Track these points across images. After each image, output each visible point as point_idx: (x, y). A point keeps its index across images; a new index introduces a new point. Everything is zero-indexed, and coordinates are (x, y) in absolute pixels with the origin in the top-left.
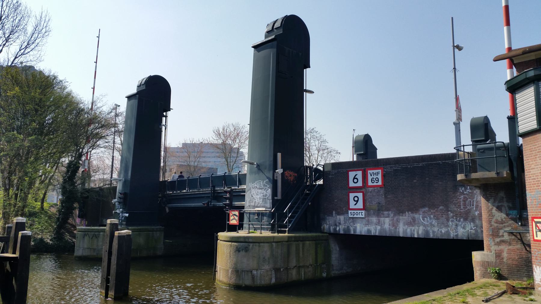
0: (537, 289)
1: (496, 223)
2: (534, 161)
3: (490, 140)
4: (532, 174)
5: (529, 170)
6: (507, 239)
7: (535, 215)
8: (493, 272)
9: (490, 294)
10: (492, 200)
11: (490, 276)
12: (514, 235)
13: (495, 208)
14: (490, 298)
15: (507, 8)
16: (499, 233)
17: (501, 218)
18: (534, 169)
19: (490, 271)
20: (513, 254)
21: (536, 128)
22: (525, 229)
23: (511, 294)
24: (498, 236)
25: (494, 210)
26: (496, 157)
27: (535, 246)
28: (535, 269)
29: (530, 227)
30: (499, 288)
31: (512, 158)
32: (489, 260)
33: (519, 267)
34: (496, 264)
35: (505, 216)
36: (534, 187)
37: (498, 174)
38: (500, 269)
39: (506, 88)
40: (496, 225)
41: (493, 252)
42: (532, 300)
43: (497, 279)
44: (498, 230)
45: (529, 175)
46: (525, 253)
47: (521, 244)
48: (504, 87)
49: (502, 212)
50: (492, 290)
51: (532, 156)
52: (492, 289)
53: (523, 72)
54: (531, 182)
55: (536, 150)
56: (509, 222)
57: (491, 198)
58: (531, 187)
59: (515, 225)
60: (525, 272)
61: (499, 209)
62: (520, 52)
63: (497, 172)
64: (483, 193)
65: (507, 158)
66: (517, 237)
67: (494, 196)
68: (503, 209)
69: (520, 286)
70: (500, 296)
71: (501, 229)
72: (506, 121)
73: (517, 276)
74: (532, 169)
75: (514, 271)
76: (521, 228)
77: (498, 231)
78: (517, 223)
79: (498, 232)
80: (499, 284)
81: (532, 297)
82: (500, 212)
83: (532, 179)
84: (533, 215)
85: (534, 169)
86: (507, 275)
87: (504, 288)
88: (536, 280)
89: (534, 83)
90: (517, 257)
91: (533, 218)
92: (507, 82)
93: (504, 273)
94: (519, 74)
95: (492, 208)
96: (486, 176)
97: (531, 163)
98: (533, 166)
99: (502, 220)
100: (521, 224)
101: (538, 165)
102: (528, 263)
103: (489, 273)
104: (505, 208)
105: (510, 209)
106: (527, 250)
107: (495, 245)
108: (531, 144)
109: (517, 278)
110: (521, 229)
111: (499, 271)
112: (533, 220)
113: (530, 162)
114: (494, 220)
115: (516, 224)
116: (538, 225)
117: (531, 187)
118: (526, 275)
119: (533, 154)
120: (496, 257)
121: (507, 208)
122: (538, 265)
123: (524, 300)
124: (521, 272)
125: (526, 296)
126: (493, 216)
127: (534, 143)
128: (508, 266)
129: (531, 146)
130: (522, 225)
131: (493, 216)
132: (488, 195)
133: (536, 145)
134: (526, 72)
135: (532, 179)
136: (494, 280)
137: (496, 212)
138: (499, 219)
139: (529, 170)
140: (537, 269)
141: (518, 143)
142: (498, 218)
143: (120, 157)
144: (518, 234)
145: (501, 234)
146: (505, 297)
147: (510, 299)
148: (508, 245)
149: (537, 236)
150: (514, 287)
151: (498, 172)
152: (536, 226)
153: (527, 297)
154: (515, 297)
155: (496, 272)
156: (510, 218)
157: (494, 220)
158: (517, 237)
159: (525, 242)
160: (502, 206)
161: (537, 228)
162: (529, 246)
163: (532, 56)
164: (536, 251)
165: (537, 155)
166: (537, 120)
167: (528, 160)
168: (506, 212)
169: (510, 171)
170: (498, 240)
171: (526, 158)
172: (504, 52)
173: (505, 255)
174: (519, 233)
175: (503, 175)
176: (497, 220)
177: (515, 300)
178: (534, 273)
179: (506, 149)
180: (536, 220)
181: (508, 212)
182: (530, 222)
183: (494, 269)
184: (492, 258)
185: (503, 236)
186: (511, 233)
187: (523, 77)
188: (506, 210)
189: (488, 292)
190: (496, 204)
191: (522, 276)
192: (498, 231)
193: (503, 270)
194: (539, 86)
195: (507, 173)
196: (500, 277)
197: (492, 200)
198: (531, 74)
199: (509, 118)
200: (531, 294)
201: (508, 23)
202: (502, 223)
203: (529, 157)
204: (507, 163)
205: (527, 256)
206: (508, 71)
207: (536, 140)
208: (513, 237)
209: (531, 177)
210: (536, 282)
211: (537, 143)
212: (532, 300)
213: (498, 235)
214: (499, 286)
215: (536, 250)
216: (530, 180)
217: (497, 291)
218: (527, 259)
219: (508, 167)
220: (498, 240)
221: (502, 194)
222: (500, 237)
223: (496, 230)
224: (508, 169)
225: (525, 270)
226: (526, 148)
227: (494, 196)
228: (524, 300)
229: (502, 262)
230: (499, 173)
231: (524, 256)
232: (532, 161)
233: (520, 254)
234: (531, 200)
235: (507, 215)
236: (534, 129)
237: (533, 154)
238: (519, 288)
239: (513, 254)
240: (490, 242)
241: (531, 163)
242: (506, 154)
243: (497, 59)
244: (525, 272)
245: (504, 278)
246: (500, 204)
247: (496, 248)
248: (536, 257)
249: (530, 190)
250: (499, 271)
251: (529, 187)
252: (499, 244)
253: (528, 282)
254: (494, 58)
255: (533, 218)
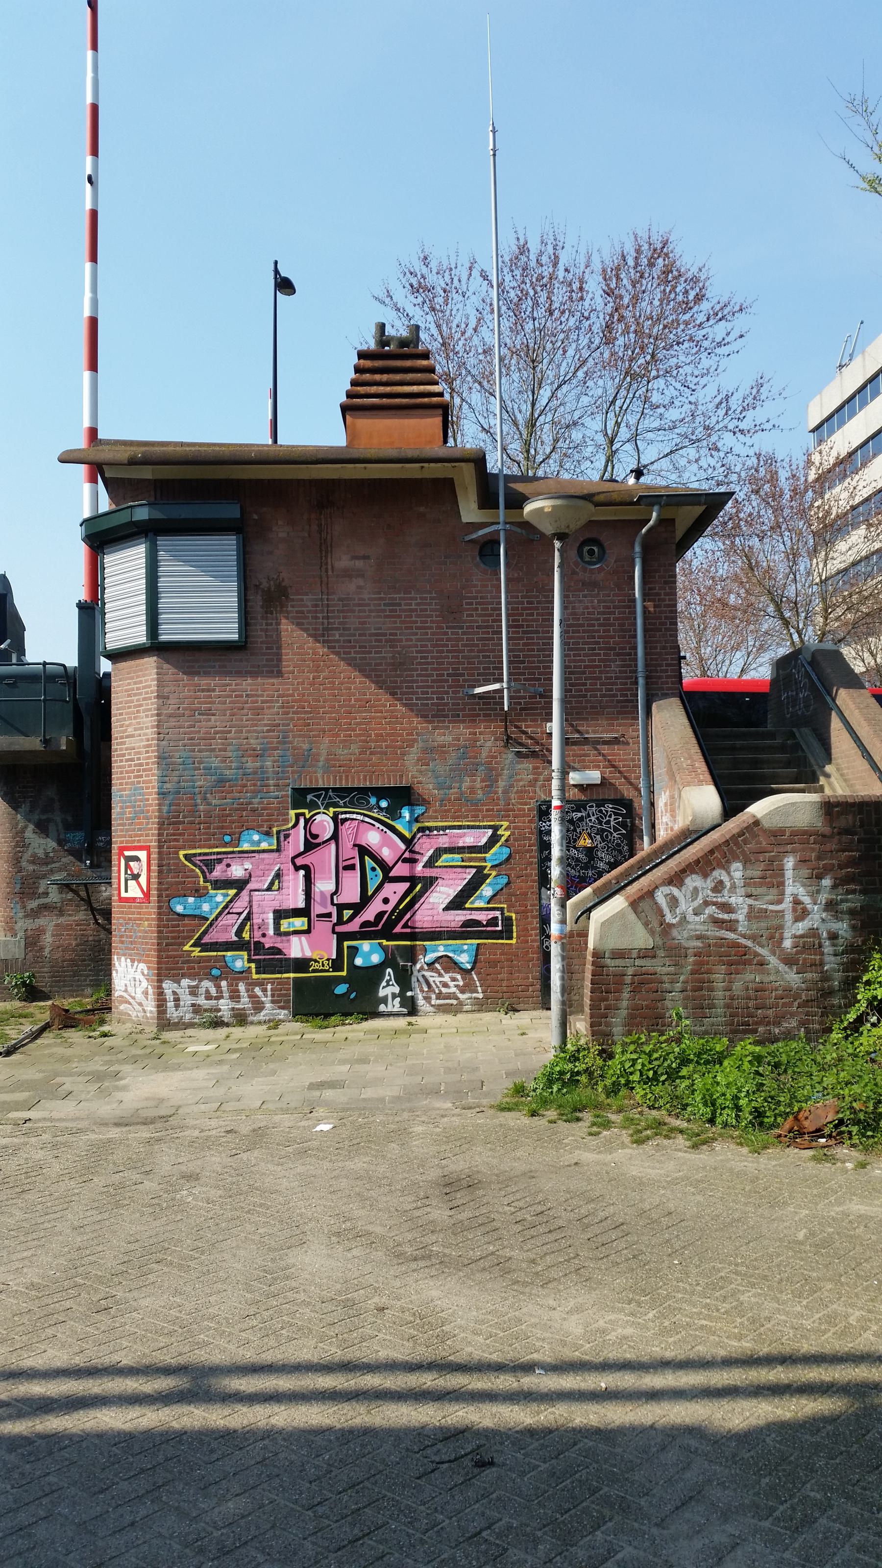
0: (117, 1008)
1: (33, 862)
2: (135, 718)
3: (9, 641)
4: (127, 749)
5: (122, 738)
6: (55, 900)
7: (127, 842)
8: (16, 984)
9: (13, 1036)
10: (25, 808)
11: (10, 994)
12: (72, 890)
13: (31, 827)
14: (16, 1044)
15: (93, 322)
16: (37, 888)
17: (44, 849)
18: (132, 736)
19: (10, 983)
20: (67, 935)
21: (144, 644)
22: (99, 874)
23: (60, 1029)
24: (34, 895)
25: (30, 832)
26: (45, 700)
27: (122, 913)
28: (117, 964)
29: (115, 869)
30: (31, 1019)
31: (82, 705)
32: (9, 957)
33: (79, 966)
34: (24, 964)
35: (54, 844)
36: (129, 778)
37: (46, 742)
38: (33, 975)
39: (84, 536)
40: (31, 868)
41: (21, 934)
42: (105, 1035)
43: (25, 1000)
44: (36, 880)
45: (121, 749)
46: (94, 930)
47: (85, 910)
48: (78, 533)
49: (47, 836)
50: (17, 1027)
51: (129, 707)
52: (16, 1025)
53: (126, 505)
54: (124, 767)
55: (141, 694)
56: (63, 859)
57: (24, 802)
58: (124, 778)
59: (77, 866)
60: (90, 975)
61: (42, 828)
62: (123, 455)
63: (44, 736)
64: (5, 788)
65: (71, 705)
66: (79, 895)
67: (31, 797)
68: (52, 828)
69: (79, 1009)
70: (36, 1038)
71: (44, 877)
72: (73, 616)
73: (72, 986)
74: (127, 737)
75: (65, 977)
76: (89, 872)
77: (34, 883)
78: (81, 860)
79: (35, 886)
80: (31, 1010)
81: (106, 1028)
82: (42, 835)
83: (127, 760)
84: (122, 842)
85: (132, 736)
86: (50, 986)
87: (46, 1017)
88: (117, 988)
89: (146, 536)
90: (74, 943)
91: (122, 849)
92: (85, 522)
93: (43, 983)
94: (114, 507)
95: (26, 827)
96: (17, 748)
97: (127, 723)
98: (130, 730)
99: (46, 854)
100: (91, 863)
101: (142, 729)
102: (97, 954)
103: (6, 988)
104: (57, 825)
105: (68, 827)
106: (98, 924)
107: (26, 917)
108: (132, 678)
109: (69, 991)
110: (89, 875)
111: (31, 981)
112: (121, 853)
113: (124, 720)
114: (27, 856)
115: (79, 863)
116: (132, 864)
117: (124, 778)
118: (91, 980)
119: (132, 702)
120: (26, 948)
121: (61, 826)
122: (124, 955)
123: (90, 1037)
124: (81, 975)
125: (92, 1028)
126: (26, 846)
127: (138, 677)
128: (52, 967)
129: (129, 684)
130: (92, 866)
131: (26, 846)
132: (17, 795)
133: (141, 682)
134: (131, 507)
135: (127, 760)
136: (17, 1004)
137: (34, 836)
138: (41, 853)
139: (122, 738)
140: (120, 965)
141: (96, 670)
142: (36, 851)
143: (71, 857)
144: (82, 887)
145: (41, 890)
146: (47, 1039)
147: (59, 1040)
148: (57, 915)
149: (126, 891)
150: (67, 1011)
151: (48, 737)
152: (127, 866)
153: (94, 1030)
154: (74, 1035)
155: (24, 984)
156: (67, 850)
157: (27, 856)
158: (79, 895)
159: (95, 906)
160: (49, 820)
161: (129, 872)
162: (107, 914)
163: (146, 473)
164: (121, 925)
165: (141, 705)
166: (147, 624)
167: (121, 714)
168: (59, 835)
169: (75, 736)
170: (33, 904)
171: (118, 709)
172: (80, 442)
173: (48, 939)
174: (86, 885)
175: (59, 745)
176: (34, 855)
177: (70, 1040)
178: (114, 974)
179: (69, 683)
180: (127, 853)
181: (62, 837)
182: (114, 858)
183: (19, 977)
184: (17, 950)
185: (46, 894)
186: (66, 887)
187: (123, 518)
188: (58, 831)
189: (6, 1032)
190: (36, 817)
191: (81, 986)
192: (34, 883)
193: (40, 977)
194: (156, 545)
195: (68, 741)
196: (32, 993)
197: (25, 808)
198: (142, 514)
199: (81, 606)
200: (102, 1022)
201: (93, 366)
202: (47, 864)
203: (124, 708)
204: (71, 716)
205: (96, 938)
206: (87, 487)
207: (141, 670)
208: (70, 895)
209: (124, 755)
210: (117, 994)
211: (143, 679)
212: (105, 1035)
213: (34, 893)
214: (31, 1015)
215: (121, 921)
216: (121, 761)
217: (28, 1028)
218: (97, 944)
219: (71, 726)
220: (33, 904)
221: (51, 792)
222: (39, 898)
223: (31, 881)
224: (71, 730)
225: (90, 970)
226: (118, 686)
227: (31, 797)
228: (90, 1037)
229: (38, 959)
230: (50, 740)
231: (91, 938)
232: (130, 718)
233: (82, 935)
234: (122, 808)
235: (60, 843)
236: (139, 645)
237: (132, 702)
238: (76, 1013)
239: (67, 935)
240: (14, 911)
241: (127, 723)
242: (69, 696)
243: (67, 458)
244: (90, 975)
245: (45, 997)
246: (44, 817)
247: (30, 924)
248: (122, 936)
249: (121, 784)
250: (31, 981)
251: (118, 779)
252: (34, 914)
253: (94, 998)
254: (61, 455)
255: (122, 849)
